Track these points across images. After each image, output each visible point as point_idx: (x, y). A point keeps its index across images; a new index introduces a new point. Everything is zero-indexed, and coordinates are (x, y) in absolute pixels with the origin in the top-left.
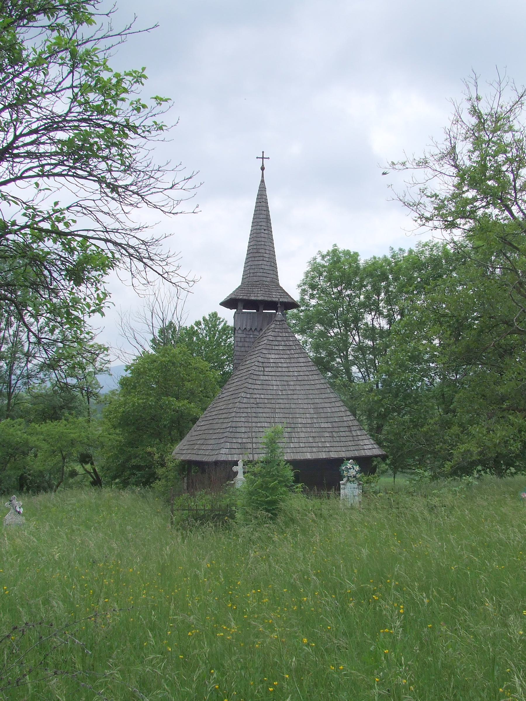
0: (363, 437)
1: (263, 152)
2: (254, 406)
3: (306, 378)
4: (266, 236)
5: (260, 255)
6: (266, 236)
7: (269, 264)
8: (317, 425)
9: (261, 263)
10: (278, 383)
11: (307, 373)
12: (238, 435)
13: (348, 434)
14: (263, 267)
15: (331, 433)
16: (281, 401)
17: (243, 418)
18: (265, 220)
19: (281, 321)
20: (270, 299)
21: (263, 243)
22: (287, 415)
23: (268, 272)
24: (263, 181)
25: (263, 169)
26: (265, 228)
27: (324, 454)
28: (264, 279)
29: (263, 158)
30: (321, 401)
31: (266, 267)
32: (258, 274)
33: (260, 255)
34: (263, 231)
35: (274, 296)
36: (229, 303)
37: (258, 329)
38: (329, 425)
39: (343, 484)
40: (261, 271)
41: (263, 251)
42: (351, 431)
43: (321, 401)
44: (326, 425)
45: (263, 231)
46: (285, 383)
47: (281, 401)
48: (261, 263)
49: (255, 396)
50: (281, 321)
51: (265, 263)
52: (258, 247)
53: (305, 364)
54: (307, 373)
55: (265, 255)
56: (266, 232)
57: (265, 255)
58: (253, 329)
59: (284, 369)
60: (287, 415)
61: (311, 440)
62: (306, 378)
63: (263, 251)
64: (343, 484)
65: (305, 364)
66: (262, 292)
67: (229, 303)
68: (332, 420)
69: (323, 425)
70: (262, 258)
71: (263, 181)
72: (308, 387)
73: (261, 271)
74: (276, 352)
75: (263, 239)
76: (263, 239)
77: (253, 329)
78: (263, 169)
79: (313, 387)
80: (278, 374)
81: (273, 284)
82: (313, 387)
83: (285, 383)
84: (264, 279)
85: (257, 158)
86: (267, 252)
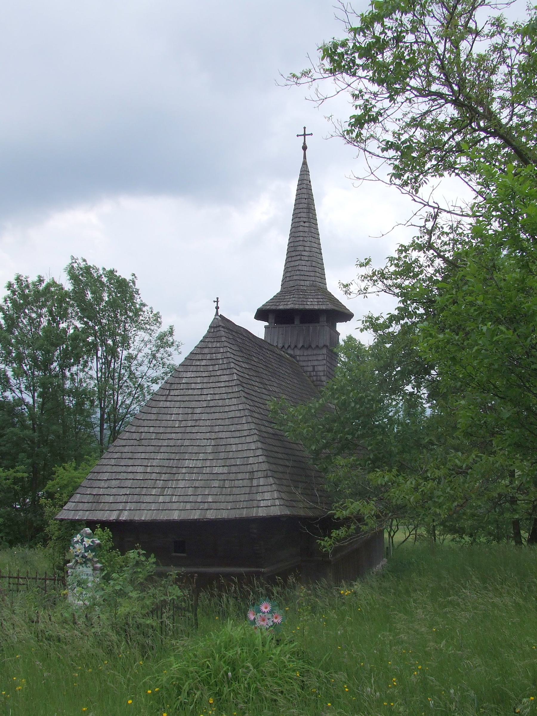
0: (265, 489)
1: (305, 128)
2: (136, 443)
3: (220, 403)
4: (306, 229)
5: (297, 253)
6: (306, 229)
7: (308, 264)
8: (208, 470)
9: (297, 263)
10: (181, 411)
11: (225, 396)
12: (97, 484)
13: (246, 483)
14: (300, 268)
15: (222, 482)
16: (173, 436)
17: (113, 460)
18: (305, 210)
19: (216, 327)
20: (301, 307)
21: (301, 239)
22: (173, 456)
23: (307, 274)
24: (305, 163)
25: (305, 148)
26: (305, 220)
27: (198, 512)
28: (302, 283)
29: (305, 135)
30: (228, 434)
31: (305, 268)
32: (295, 278)
33: (297, 253)
34: (302, 224)
35: (308, 303)
36: (261, 315)
37: (293, 346)
38: (225, 470)
39: (71, 568)
40: (298, 273)
41: (301, 248)
42: (252, 479)
43: (228, 434)
44: (220, 470)
45: (302, 224)
46: (190, 411)
47: (173, 436)
48: (297, 263)
49: (142, 430)
50: (216, 327)
51: (303, 263)
52: (296, 244)
53: (227, 384)
54: (225, 396)
55: (304, 253)
56: (307, 224)
57: (304, 253)
58: (286, 347)
59: (196, 392)
60: (173, 456)
61: (190, 491)
62: (220, 403)
63: (301, 248)
64: (71, 568)
65: (227, 384)
66: (294, 299)
67: (261, 315)
68: (228, 462)
69: (216, 470)
70: (299, 258)
71: (305, 163)
72: (217, 416)
73: (298, 273)
74: (195, 369)
75: (302, 234)
76: (302, 234)
77: (286, 347)
78: (305, 148)
79: (225, 415)
80: (187, 398)
81: (313, 288)
82: (225, 415)
83: (190, 411)
84: (302, 283)
85: (298, 136)
86: (307, 249)
